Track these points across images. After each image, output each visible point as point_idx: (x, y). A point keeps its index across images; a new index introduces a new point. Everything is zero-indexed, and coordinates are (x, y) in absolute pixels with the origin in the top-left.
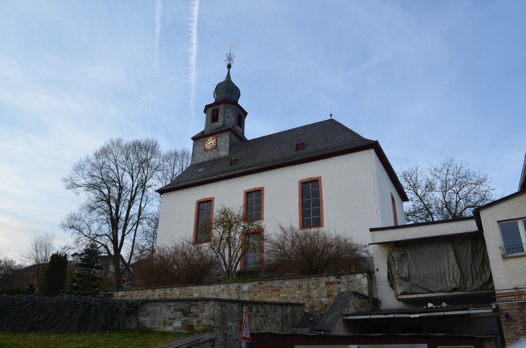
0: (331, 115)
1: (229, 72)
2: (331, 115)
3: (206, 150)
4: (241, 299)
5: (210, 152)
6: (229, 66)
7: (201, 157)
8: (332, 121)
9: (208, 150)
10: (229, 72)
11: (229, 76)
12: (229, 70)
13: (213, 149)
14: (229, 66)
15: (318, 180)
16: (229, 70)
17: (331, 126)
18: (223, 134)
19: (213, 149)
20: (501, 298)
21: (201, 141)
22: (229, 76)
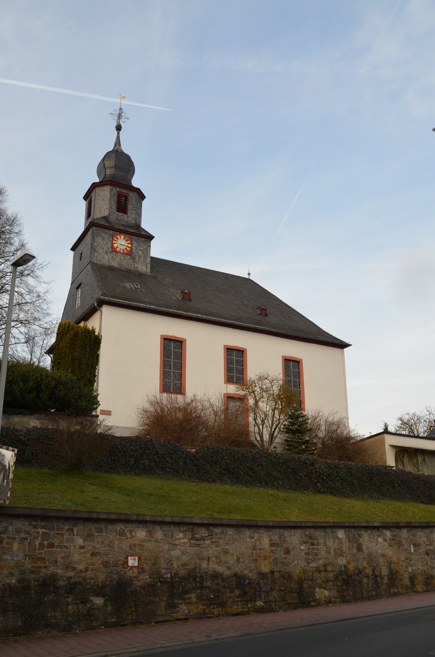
0: (249, 274)
1: (118, 138)
2: (249, 274)
3: (114, 250)
4: (193, 522)
5: (119, 256)
6: (119, 128)
7: (106, 257)
8: (249, 280)
9: (117, 252)
10: (118, 138)
11: (118, 142)
12: (118, 134)
13: (126, 254)
14: (119, 128)
15: (181, 342)
16: (118, 134)
17: (246, 286)
18: (141, 239)
19: (126, 254)
20: (128, 649)
21: (106, 234)
22: (118, 142)
